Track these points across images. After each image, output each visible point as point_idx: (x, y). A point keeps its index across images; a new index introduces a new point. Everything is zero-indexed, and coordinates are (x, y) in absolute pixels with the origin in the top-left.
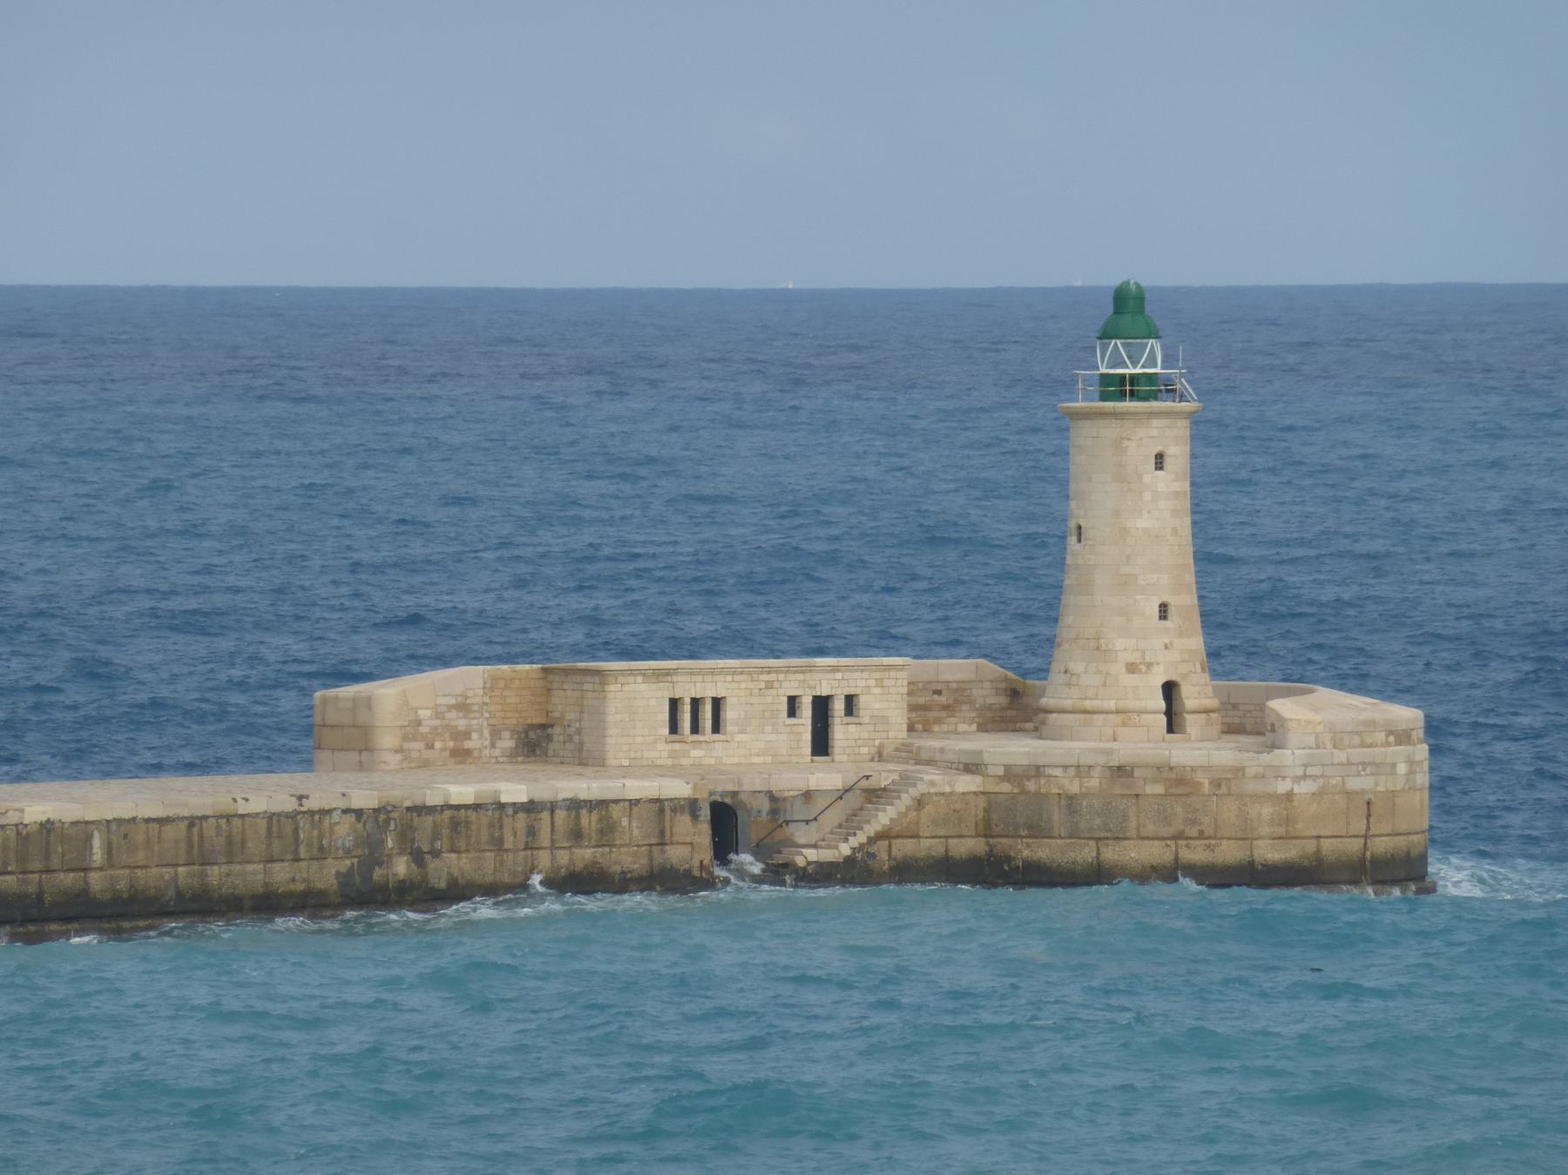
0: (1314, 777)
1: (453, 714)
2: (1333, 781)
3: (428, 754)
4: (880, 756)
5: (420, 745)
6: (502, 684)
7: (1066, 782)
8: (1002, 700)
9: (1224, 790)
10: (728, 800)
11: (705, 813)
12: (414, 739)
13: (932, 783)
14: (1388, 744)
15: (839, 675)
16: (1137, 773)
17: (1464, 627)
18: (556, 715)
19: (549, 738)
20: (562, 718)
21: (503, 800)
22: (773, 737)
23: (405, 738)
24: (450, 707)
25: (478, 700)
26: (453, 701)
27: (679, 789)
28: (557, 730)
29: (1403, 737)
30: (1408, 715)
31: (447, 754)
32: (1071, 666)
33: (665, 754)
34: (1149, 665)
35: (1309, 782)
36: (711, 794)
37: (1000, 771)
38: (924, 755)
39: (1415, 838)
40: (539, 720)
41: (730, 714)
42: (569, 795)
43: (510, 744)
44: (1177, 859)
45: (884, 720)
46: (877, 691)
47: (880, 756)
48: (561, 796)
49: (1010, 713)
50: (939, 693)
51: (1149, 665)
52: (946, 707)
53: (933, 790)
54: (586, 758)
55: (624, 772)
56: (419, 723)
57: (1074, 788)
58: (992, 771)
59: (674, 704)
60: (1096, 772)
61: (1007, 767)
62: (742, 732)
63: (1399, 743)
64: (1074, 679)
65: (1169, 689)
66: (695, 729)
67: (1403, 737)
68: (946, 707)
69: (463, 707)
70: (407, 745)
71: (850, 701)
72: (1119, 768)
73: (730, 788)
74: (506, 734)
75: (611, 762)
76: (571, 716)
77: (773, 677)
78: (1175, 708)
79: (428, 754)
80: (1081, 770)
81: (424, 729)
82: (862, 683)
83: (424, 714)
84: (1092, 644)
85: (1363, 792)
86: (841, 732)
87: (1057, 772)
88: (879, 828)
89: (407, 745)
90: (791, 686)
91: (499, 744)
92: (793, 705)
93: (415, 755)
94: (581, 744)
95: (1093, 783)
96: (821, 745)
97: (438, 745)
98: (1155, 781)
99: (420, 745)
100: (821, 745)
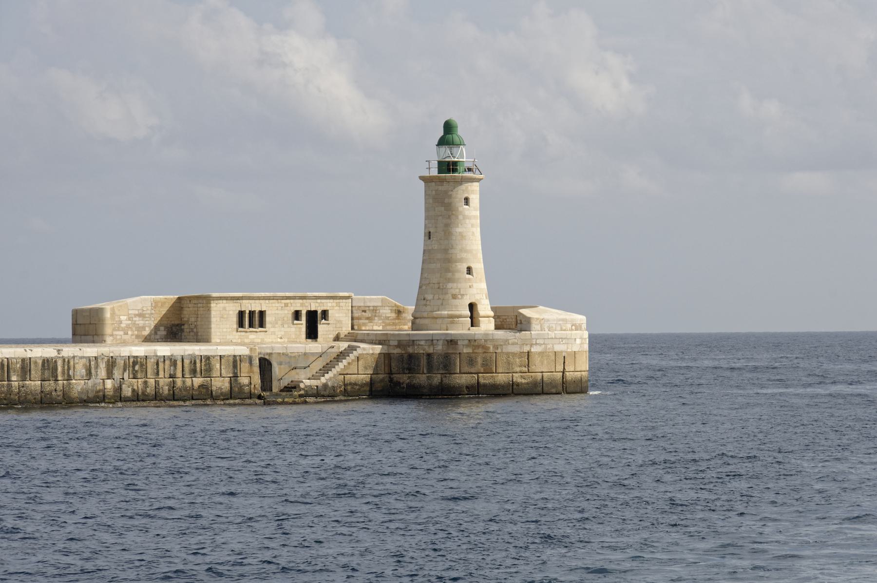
0: (540, 345)
1: (137, 319)
2: (549, 346)
3: (126, 337)
4: (337, 338)
5: (121, 333)
6: (160, 305)
7: (426, 347)
8: (394, 315)
9: (499, 351)
10: (267, 357)
11: (256, 362)
12: (119, 330)
13: (364, 349)
14: (572, 330)
15: (319, 301)
16: (459, 343)
17: (514, 477)
18: (185, 319)
19: (182, 330)
20: (188, 321)
21: (159, 354)
22: (289, 330)
23: (114, 330)
24: (136, 315)
25: (149, 312)
26: (137, 312)
27: (243, 351)
28: (186, 326)
29: (578, 327)
30: (581, 319)
31: (134, 337)
32: (426, 296)
33: (237, 337)
34: (463, 295)
35: (538, 347)
36: (260, 353)
37: (396, 343)
38: (359, 337)
39: (583, 373)
40: (177, 322)
41: (268, 319)
42: (191, 353)
43: (164, 333)
44: (478, 383)
45: (340, 322)
46: (337, 308)
47: (337, 338)
48: (187, 353)
49: (397, 321)
50: (364, 311)
51: (463, 295)
52: (368, 318)
53: (365, 352)
54: (201, 337)
55: (218, 344)
56: (121, 322)
57: (431, 351)
58: (392, 343)
59: (241, 314)
60: (441, 343)
61: (399, 341)
62: (274, 327)
63: (576, 330)
64: (428, 303)
65: (472, 307)
66: (251, 326)
67: (578, 327)
68: (368, 318)
69: (141, 315)
70: (115, 333)
71: (325, 314)
72: (451, 341)
73: (269, 351)
74: (162, 328)
75: (213, 341)
76: (193, 319)
77: (288, 301)
78: (475, 315)
79: (126, 337)
80: (432, 341)
81: (123, 325)
82: (330, 305)
83: (123, 318)
84: (436, 286)
85: (562, 352)
86: (322, 328)
87: (422, 343)
88: (339, 370)
89: (115, 333)
90: (297, 305)
91: (159, 333)
92: (297, 315)
93: (118, 337)
94: (197, 332)
95: (439, 347)
96: (312, 333)
97: (130, 333)
98: (467, 346)
99: (121, 333)
100: (312, 333)
